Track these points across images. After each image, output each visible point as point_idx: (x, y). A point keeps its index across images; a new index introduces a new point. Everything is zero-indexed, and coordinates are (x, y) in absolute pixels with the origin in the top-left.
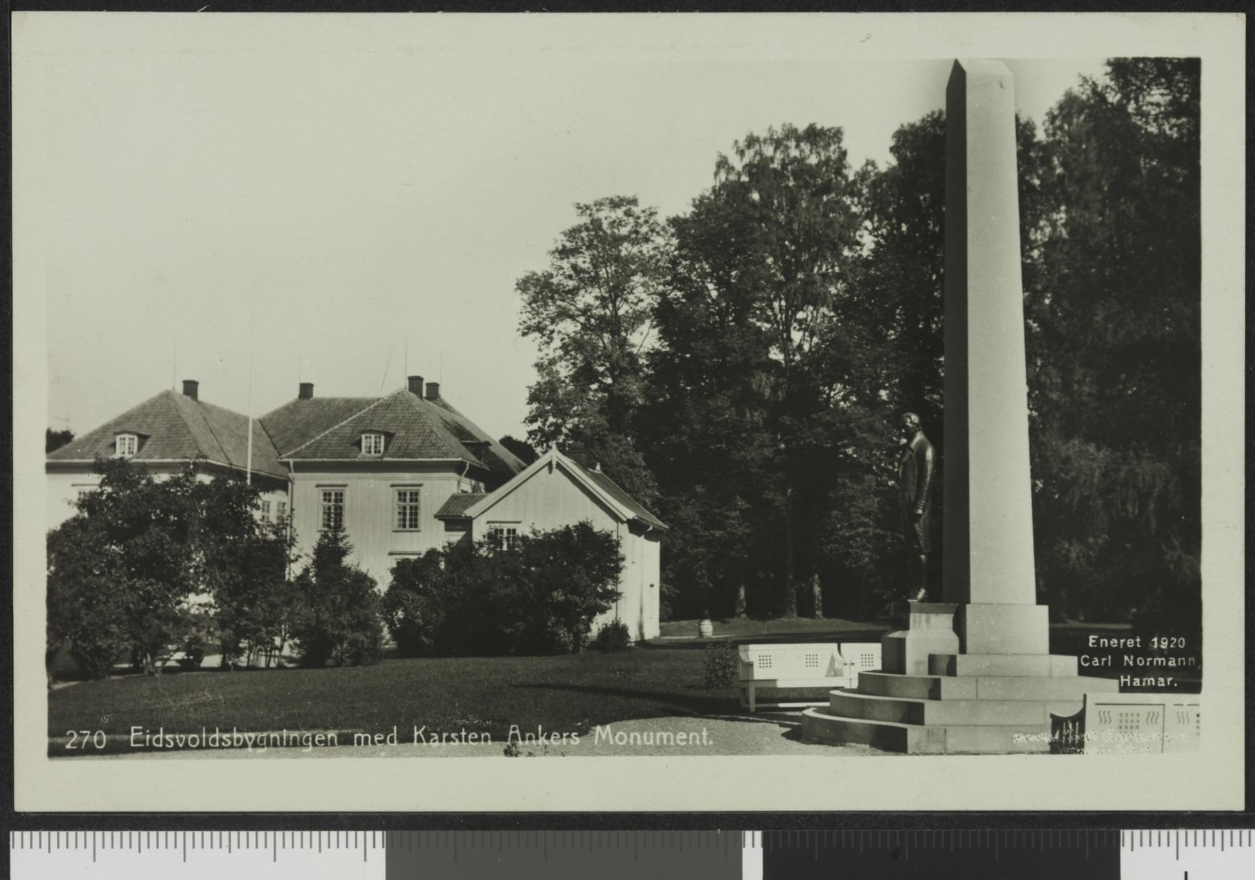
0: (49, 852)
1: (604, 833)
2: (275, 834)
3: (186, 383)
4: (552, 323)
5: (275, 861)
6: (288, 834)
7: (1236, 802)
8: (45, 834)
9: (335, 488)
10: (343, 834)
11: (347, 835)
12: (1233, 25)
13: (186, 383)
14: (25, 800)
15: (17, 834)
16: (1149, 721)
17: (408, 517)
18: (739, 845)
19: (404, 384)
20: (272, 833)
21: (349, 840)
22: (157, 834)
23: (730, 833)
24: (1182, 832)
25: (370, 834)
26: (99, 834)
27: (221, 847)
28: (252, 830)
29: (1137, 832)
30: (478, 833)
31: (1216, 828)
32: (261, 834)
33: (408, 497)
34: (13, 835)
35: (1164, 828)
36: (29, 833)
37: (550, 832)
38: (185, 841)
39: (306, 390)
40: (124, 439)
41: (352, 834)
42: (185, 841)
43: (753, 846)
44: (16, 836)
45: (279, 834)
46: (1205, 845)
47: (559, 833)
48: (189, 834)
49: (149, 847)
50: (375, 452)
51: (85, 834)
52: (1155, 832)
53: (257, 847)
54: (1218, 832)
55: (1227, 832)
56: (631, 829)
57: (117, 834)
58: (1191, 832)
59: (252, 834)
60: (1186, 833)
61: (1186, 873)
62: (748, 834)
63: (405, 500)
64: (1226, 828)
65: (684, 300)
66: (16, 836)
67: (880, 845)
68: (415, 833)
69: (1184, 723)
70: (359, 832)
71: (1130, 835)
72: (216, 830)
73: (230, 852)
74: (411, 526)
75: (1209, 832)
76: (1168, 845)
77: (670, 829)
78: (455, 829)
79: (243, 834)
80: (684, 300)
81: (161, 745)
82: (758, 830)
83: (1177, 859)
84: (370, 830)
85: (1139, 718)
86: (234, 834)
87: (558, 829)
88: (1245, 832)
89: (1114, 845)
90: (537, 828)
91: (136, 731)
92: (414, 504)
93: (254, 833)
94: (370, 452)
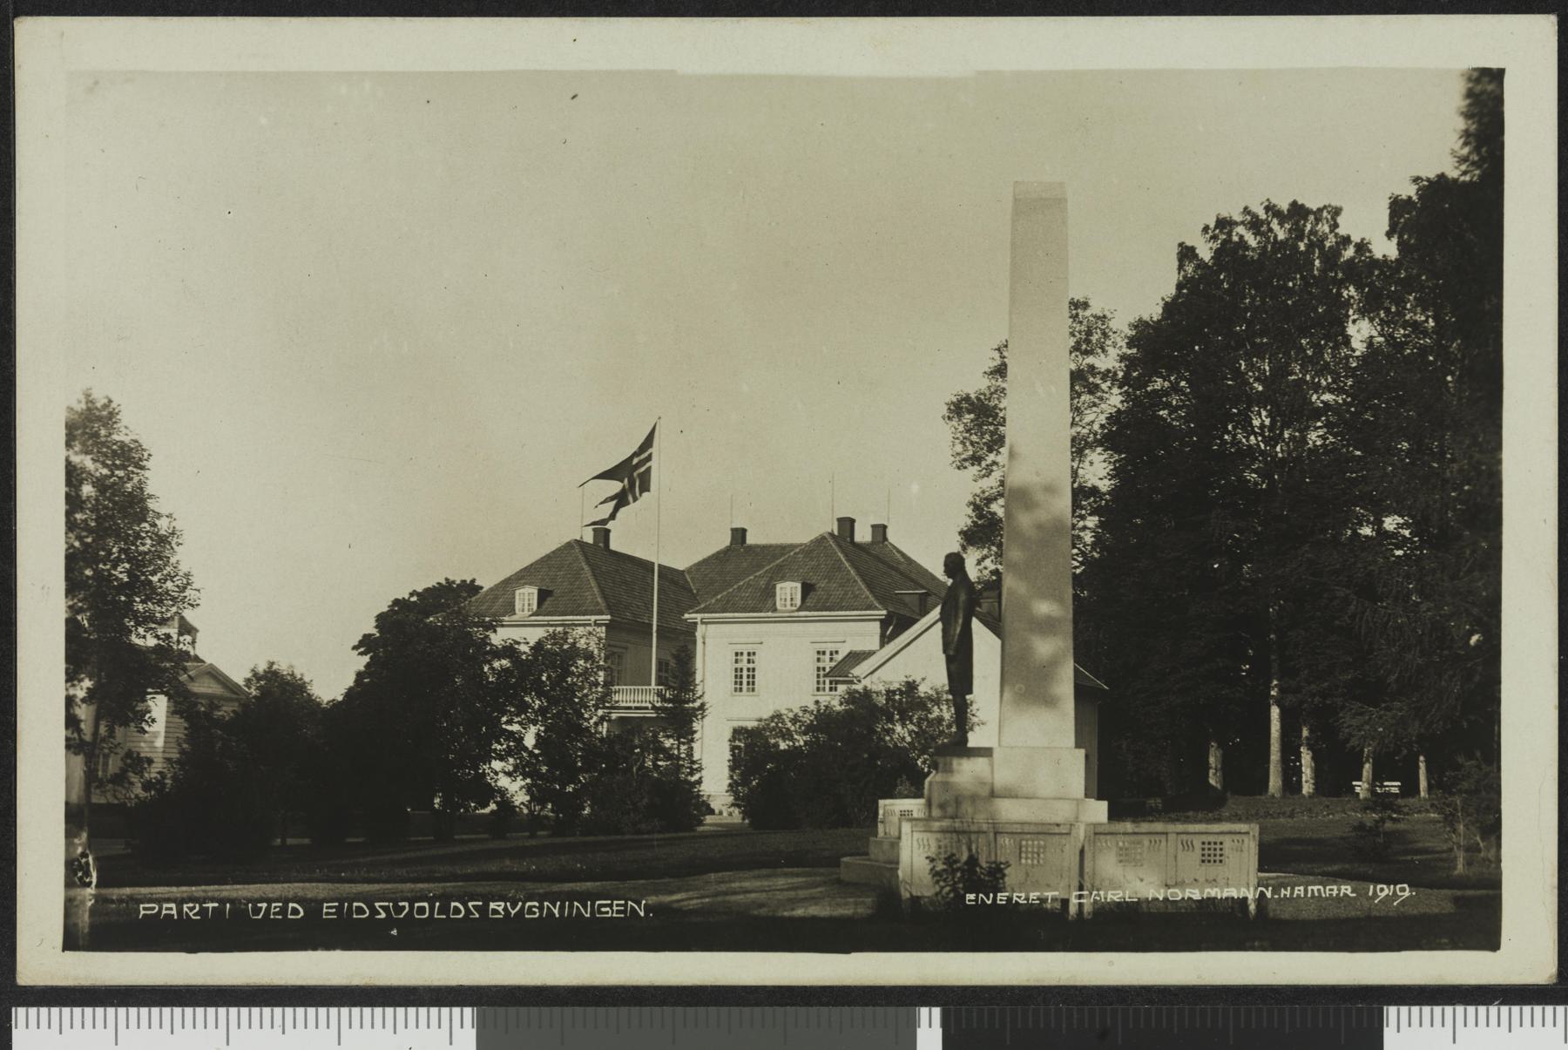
2: (150, 1010)
3: (734, 531)
4: (990, 450)
6: (356, 1011)
9: (829, 645)
10: (423, 1010)
11: (428, 1012)
12: (1541, 29)
13: (734, 531)
15: (21, 1011)
16: (1152, 849)
17: (745, 680)
18: (913, 1024)
23: (902, 1010)
24: (1460, 1009)
27: (272, 1027)
29: (1404, 1009)
34: (16, 1010)
37: (679, 1010)
39: (739, 534)
40: (524, 594)
41: (434, 1010)
44: (20, 1013)
45: (401, 1011)
46: (1488, 1026)
47: (690, 1010)
50: (792, 605)
51: (105, 1011)
52: (1426, 1009)
53: (94, 1027)
60: (1465, 1010)
62: (924, 1011)
66: (20, 1013)
69: (1188, 850)
73: (284, 1033)
74: (748, 690)
77: (827, 1004)
79: (300, 1010)
81: (291, 905)
82: (937, 1006)
84: (458, 1006)
85: (1223, 852)
87: (690, 1005)
89: (1376, 1026)
90: (663, 1003)
93: (213, 1009)
94: (785, 606)
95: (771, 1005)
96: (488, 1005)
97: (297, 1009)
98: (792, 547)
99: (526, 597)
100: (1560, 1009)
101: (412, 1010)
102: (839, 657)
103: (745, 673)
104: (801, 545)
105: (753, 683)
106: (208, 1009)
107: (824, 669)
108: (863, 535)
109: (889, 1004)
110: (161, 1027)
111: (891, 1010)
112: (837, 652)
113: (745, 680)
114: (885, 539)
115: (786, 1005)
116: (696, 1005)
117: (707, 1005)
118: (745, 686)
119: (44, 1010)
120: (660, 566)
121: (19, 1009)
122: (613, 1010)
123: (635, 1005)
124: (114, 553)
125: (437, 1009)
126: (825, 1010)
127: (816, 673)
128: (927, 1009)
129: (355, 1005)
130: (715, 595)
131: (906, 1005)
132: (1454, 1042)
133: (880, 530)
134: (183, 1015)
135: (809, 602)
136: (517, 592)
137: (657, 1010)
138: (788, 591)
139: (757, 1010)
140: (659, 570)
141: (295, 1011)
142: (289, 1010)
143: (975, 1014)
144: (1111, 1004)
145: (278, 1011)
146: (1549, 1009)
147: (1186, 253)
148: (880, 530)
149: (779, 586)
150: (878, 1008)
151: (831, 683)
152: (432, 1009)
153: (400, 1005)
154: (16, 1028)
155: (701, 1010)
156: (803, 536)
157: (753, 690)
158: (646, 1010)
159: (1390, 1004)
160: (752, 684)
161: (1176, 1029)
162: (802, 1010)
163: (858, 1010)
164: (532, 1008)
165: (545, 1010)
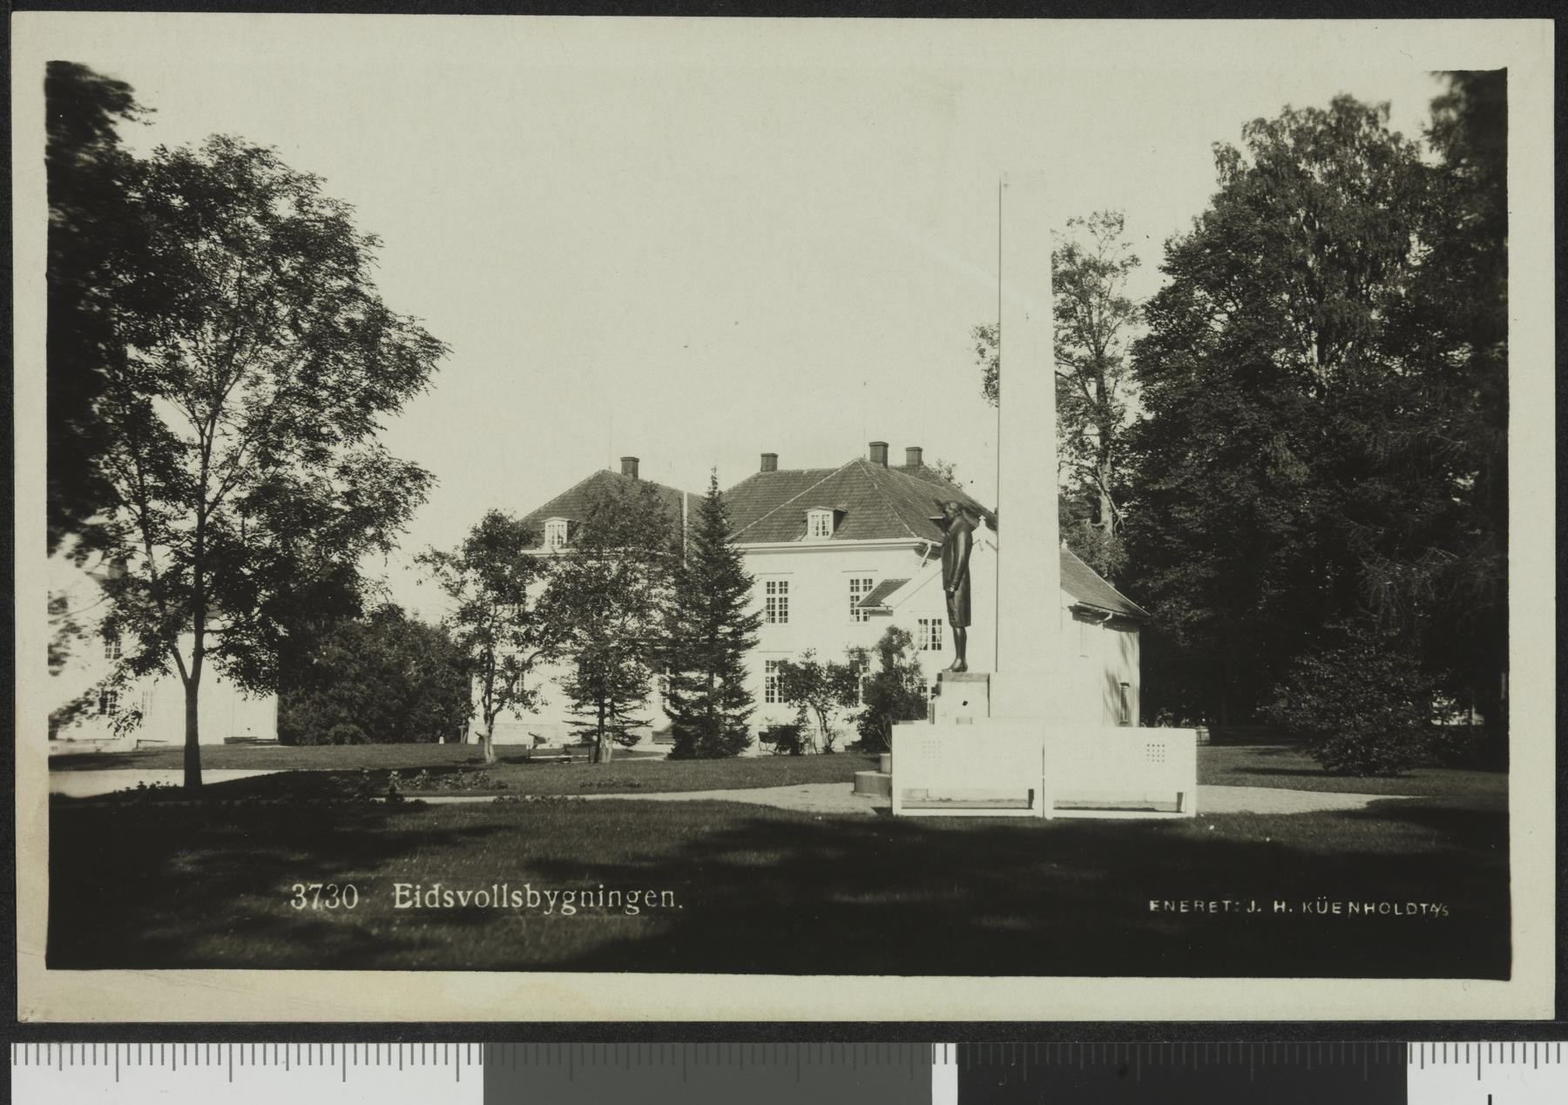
3: (625, 460)
5: (117, 1081)
6: (361, 1047)
10: (429, 1046)
11: (276, 1048)
14: (30, 1009)
15: (21, 1047)
17: (777, 610)
18: (927, 1061)
19: (866, 453)
20: (250, 1045)
23: (917, 1046)
24: (1485, 1045)
25: (463, 1046)
27: (276, 1063)
28: (316, 1042)
29: (1428, 1045)
30: (600, 1046)
32: (327, 1047)
33: (777, 588)
35: (1462, 1040)
37: (690, 1046)
38: (231, 1056)
39: (770, 459)
41: (441, 1046)
42: (231, 1056)
44: (18, 1050)
47: (702, 1046)
48: (236, 1046)
51: (106, 1047)
52: (1451, 1045)
54: (1530, 1045)
55: (1541, 1045)
56: (792, 1041)
58: (1496, 1045)
59: (191, 1047)
60: (1490, 1046)
61: (1490, 1097)
62: (939, 1047)
63: (774, 591)
64: (1541, 1040)
65: (98, 132)
66: (18, 1050)
68: (520, 1046)
70: (427, 1045)
73: (287, 1069)
74: (781, 621)
75: (1519, 1045)
77: (841, 1040)
78: (571, 1041)
79: (304, 1046)
80: (98, 132)
82: (952, 1042)
84: (464, 1042)
86: (293, 1047)
87: (701, 1041)
88: (1553, 1045)
90: (675, 1039)
92: (783, 596)
95: (784, 1041)
96: (496, 1042)
98: (826, 473)
99: (556, 528)
101: (418, 1046)
102: (875, 585)
103: (777, 604)
104: (831, 472)
105: (786, 613)
107: (858, 598)
108: (897, 458)
110: (106, 1064)
111: (906, 1046)
113: (777, 610)
114: (920, 462)
116: (707, 1041)
117: (718, 1041)
118: (777, 617)
119: (43, 1046)
120: (689, 495)
121: (18, 1045)
122: (622, 1046)
123: (645, 1042)
125: (443, 1045)
126: (838, 1046)
127: (850, 602)
129: (360, 1041)
130: (745, 526)
131: (922, 1041)
132: (1479, 1078)
135: (842, 527)
136: (547, 524)
137: (667, 1046)
138: (820, 517)
140: (689, 500)
141: (299, 1047)
144: (1130, 1040)
145: (282, 1047)
150: (892, 1044)
151: (865, 613)
152: (347, 1045)
154: (15, 1064)
155: (713, 1046)
156: (837, 460)
157: (786, 621)
160: (784, 615)
162: (884, 1046)
163: (872, 1046)
164: (540, 1044)
165: (554, 1046)
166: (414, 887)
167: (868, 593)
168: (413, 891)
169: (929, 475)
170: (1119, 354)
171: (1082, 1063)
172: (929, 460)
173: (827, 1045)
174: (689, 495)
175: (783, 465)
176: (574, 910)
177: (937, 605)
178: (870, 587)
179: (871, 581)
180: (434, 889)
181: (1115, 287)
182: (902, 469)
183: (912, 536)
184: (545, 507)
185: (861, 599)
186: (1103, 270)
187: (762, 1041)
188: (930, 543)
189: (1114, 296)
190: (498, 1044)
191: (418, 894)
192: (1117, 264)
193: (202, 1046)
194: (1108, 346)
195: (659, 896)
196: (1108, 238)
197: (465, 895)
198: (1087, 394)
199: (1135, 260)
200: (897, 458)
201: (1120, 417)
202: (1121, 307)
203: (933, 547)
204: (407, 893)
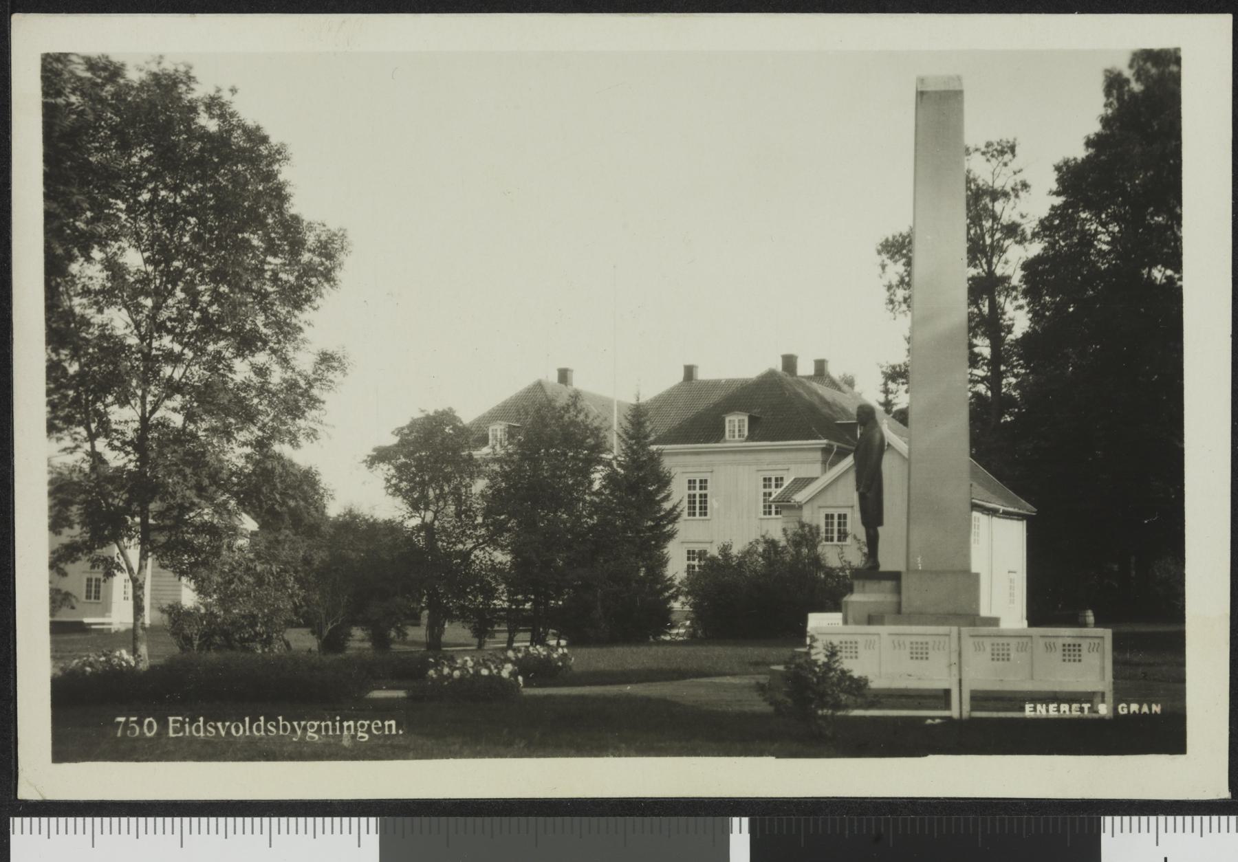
0: (31, 833)
1: (594, 820)
6: (284, 820)
7: (1222, 791)
8: (133, 820)
10: (337, 820)
11: (217, 821)
14: (26, 792)
15: (18, 820)
17: (698, 505)
18: (726, 831)
21: (201, 828)
22: (1228, 819)
23: (718, 819)
24: (1162, 818)
25: (363, 820)
26: (97, 820)
29: (1117, 819)
30: (470, 820)
31: (131, 816)
33: (698, 485)
36: (28, 819)
37: (541, 819)
38: (182, 827)
39: (689, 371)
41: (346, 820)
42: (182, 827)
43: (288, 833)
44: (16, 822)
45: (319, 820)
47: (550, 819)
48: (186, 820)
49: (111, 833)
50: (740, 436)
51: (84, 820)
56: (620, 816)
57: (115, 820)
62: (736, 820)
63: (694, 488)
66: (16, 822)
67: (785, 832)
71: (82, 822)
72: (213, 816)
75: (1188, 818)
76: (1148, 831)
82: (745, 816)
83: (182, 846)
84: (364, 816)
87: (548, 816)
89: (1095, 831)
90: (528, 814)
91: (175, 722)
92: (703, 492)
93: (250, 819)
94: (734, 437)
95: (614, 816)
96: (389, 816)
97: (140, 818)
100: (1233, 818)
101: (328, 820)
102: (786, 483)
103: (698, 499)
106: (166, 818)
109: (708, 815)
110: (129, 833)
111: (709, 819)
112: (782, 479)
113: (698, 505)
115: (627, 815)
118: (697, 511)
119: (35, 820)
121: (16, 818)
122: (488, 819)
123: (506, 816)
124: (133, 519)
125: (348, 818)
128: (738, 818)
129: (283, 816)
131: (722, 816)
132: (1157, 844)
133: (820, 366)
134: (146, 824)
137: (523, 819)
138: (736, 422)
139: (603, 820)
142: (231, 820)
143: (776, 823)
146: (1179, 818)
147: (790, 362)
148: (820, 366)
149: (727, 419)
151: (776, 508)
152: (344, 819)
153: (319, 816)
155: (559, 819)
158: (514, 819)
159: (1106, 814)
161: (936, 834)
163: (683, 819)
166: (184, 719)
167: (779, 490)
168: (183, 723)
169: (833, 384)
170: (1008, 272)
171: (847, 832)
172: (835, 371)
173: (648, 819)
174: (618, 402)
175: (702, 375)
176: (367, 736)
177: (847, 498)
178: (781, 485)
179: (782, 479)
180: (260, 721)
181: (1007, 211)
182: (809, 378)
183: (820, 439)
184: (489, 413)
185: (774, 496)
186: (995, 195)
187: (597, 816)
188: (835, 445)
189: (1005, 220)
190: (390, 818)
191: (187, 726)
192: (1008, 189)
193: (160, 820)
194: (1000, 266)
195: (383, 725)
196: (1001, 164)
197: (224, 726)
198: (980, 310)
199: (1025, 186)
200: (805, 368)
201: (1009, 329)
202: (1012, 230)
203: (838, 447)
204: (178, 725)
